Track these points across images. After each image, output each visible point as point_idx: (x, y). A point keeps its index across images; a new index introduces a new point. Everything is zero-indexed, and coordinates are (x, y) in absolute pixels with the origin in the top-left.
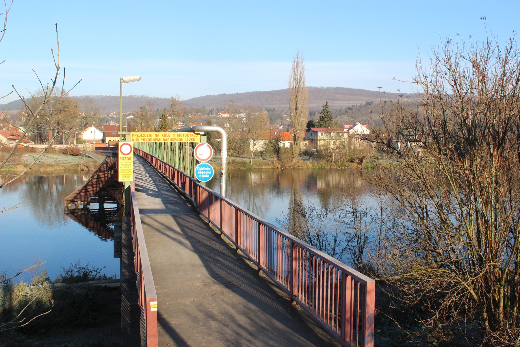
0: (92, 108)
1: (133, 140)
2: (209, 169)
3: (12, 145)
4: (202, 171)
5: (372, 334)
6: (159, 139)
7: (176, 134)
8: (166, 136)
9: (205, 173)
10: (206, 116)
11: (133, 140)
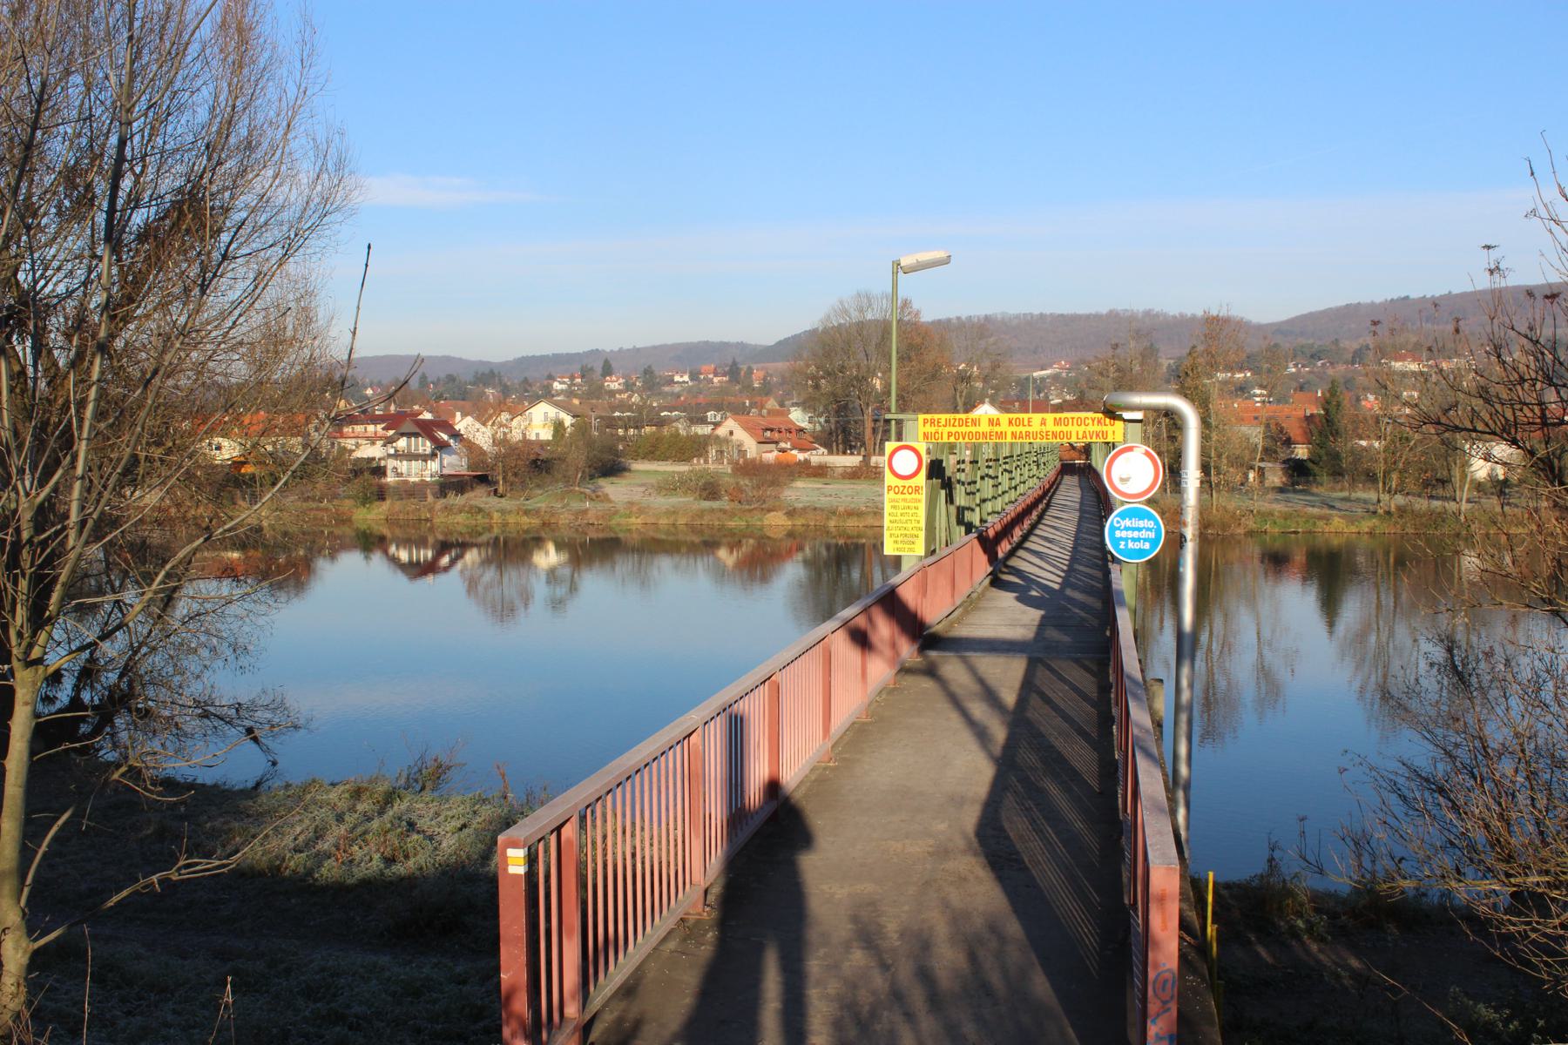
0: (986, 350)
1: (926, 435)
2: (1151, 524)
3: (771, 456)
4: (1127, 529)
5: (1171, 1037)
6: (1000, 435)
7: (1050, 417)
8: (1020, 422)
9: (1136, 534)
10: (1341, 368)
11: (926, 435)
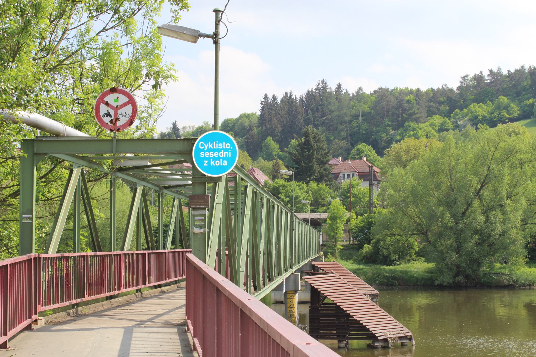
2: (228, 146)
4: (209, 150)
9: (216, 154)
